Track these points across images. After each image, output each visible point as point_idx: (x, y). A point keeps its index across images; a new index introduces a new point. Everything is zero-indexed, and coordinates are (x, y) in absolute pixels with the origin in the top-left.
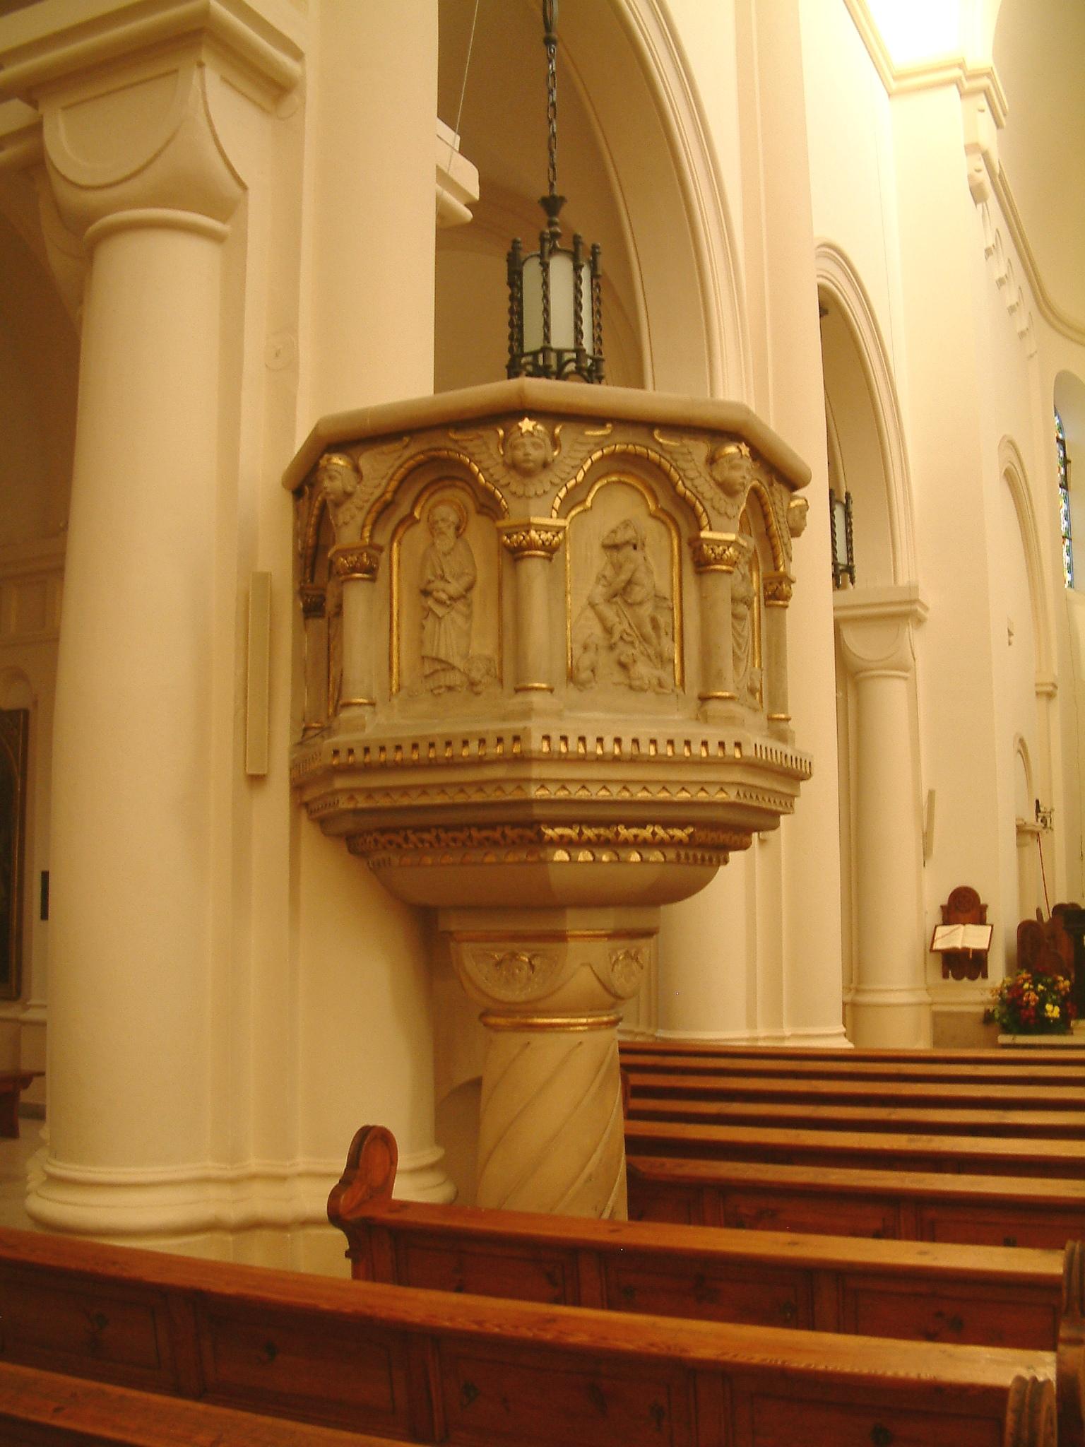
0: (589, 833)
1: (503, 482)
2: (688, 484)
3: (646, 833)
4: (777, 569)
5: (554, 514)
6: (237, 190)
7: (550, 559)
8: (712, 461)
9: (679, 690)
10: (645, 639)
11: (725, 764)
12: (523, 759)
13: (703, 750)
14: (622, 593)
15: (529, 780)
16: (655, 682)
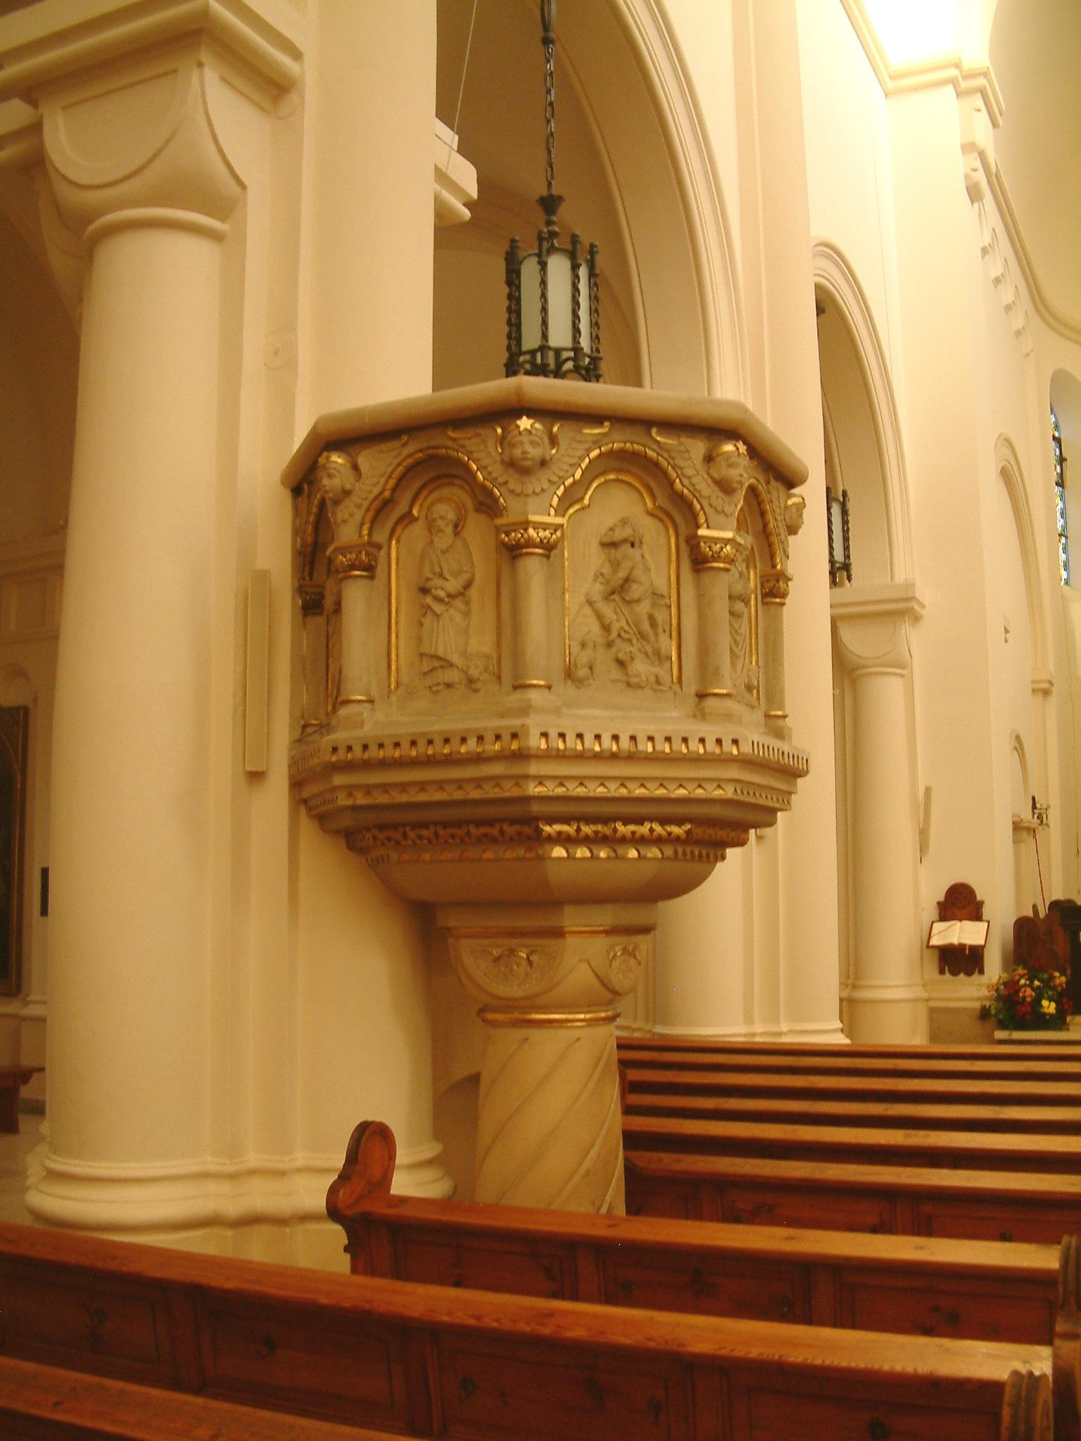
0: (587, 829)
1: (501, 480)
2: (686, 482)
3: (644, 829)
4: (774, 566)
5: (552, 512)
7: (548, 557)
8: (709, 459)
9: (676, 688)
11: (722, 760)
13: (701, 747)
14: (619, 590)
15: (527, 777)
16: (652, 679)
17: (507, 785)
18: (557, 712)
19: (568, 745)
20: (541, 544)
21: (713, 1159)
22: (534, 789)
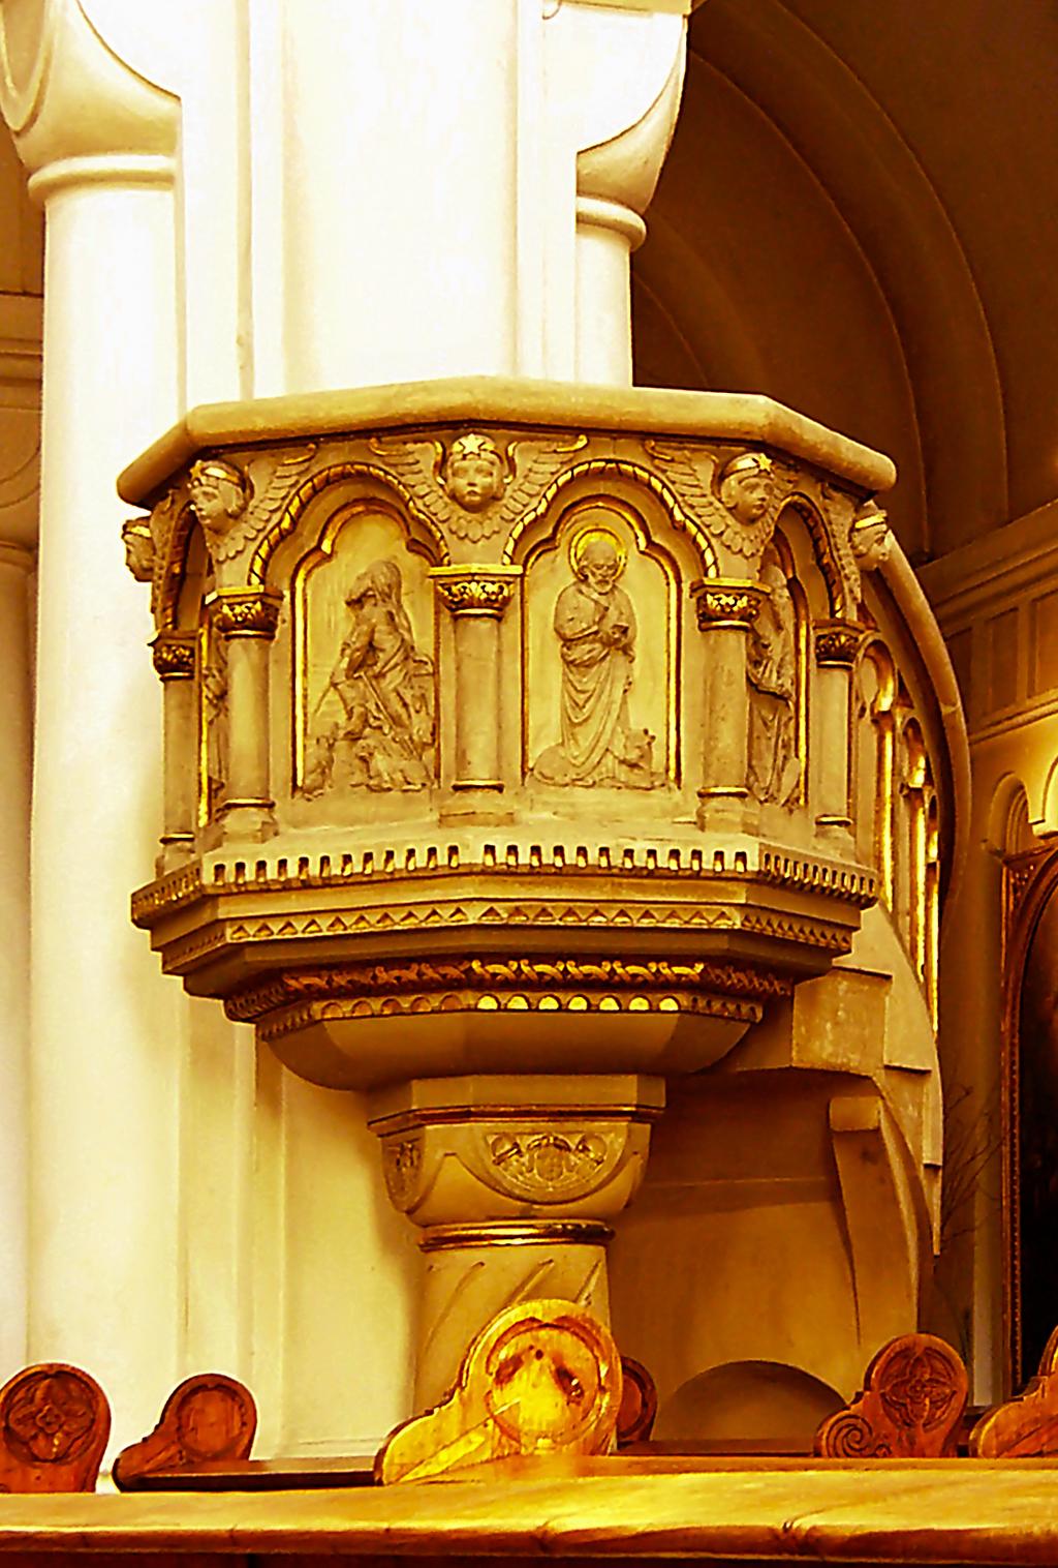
0: (341, 980)
1: (442, 516)
2: (687, 510)
3: (411, 975)
4: (833, 613)
5: (507, 560)
6: (165, 106)
7: (499, 619)
8: (720, 478)
9: (673, 785)
10: (396, 721)
11: (497, 873)
12: (206, 899)
13: (581, 859)
14: (364, 659)
15: (220, 923)
16: (399, 777)
17: (299, 925)
18: (510, 819)
19: (591, 861)
20: (488, 602)
21: (987, 1347)
22: (230, 935)
